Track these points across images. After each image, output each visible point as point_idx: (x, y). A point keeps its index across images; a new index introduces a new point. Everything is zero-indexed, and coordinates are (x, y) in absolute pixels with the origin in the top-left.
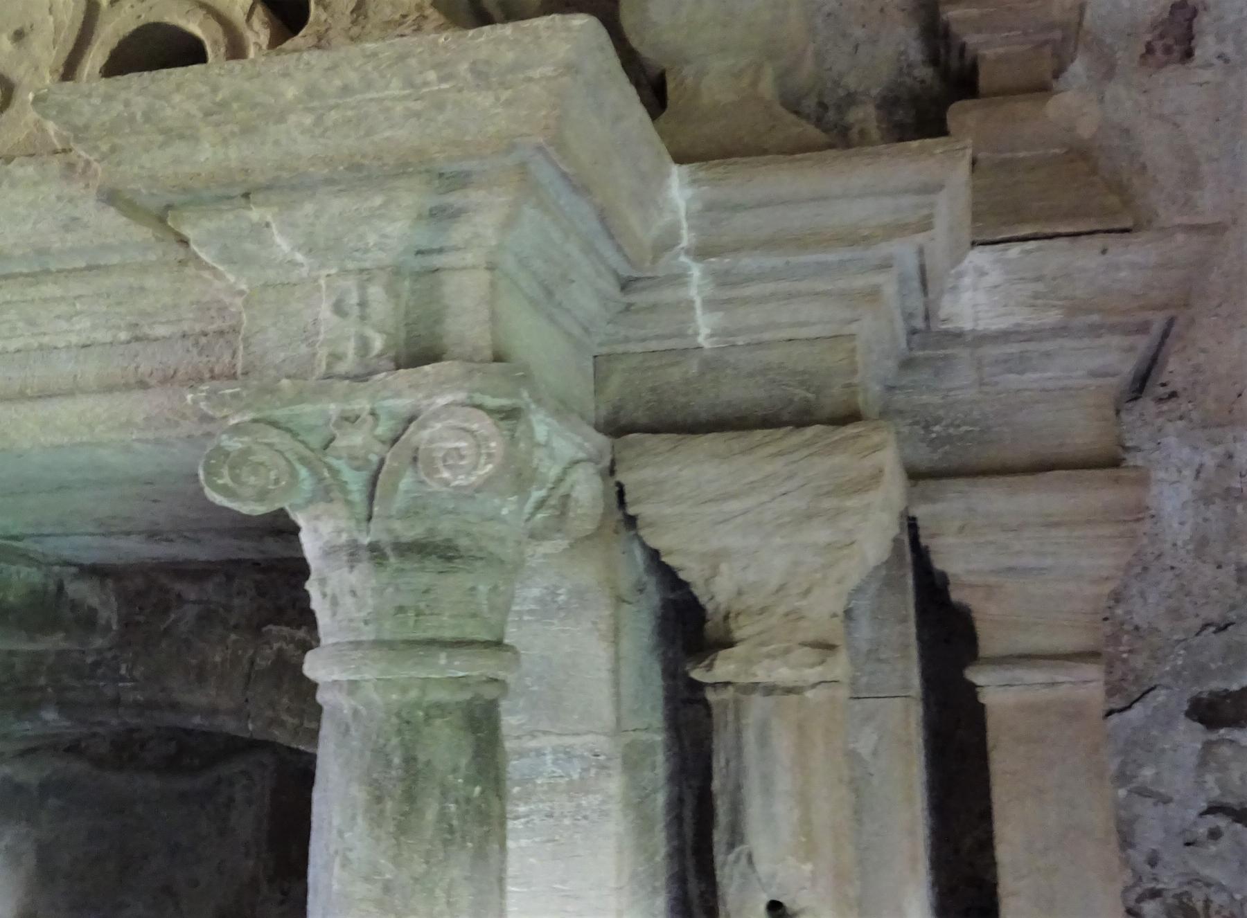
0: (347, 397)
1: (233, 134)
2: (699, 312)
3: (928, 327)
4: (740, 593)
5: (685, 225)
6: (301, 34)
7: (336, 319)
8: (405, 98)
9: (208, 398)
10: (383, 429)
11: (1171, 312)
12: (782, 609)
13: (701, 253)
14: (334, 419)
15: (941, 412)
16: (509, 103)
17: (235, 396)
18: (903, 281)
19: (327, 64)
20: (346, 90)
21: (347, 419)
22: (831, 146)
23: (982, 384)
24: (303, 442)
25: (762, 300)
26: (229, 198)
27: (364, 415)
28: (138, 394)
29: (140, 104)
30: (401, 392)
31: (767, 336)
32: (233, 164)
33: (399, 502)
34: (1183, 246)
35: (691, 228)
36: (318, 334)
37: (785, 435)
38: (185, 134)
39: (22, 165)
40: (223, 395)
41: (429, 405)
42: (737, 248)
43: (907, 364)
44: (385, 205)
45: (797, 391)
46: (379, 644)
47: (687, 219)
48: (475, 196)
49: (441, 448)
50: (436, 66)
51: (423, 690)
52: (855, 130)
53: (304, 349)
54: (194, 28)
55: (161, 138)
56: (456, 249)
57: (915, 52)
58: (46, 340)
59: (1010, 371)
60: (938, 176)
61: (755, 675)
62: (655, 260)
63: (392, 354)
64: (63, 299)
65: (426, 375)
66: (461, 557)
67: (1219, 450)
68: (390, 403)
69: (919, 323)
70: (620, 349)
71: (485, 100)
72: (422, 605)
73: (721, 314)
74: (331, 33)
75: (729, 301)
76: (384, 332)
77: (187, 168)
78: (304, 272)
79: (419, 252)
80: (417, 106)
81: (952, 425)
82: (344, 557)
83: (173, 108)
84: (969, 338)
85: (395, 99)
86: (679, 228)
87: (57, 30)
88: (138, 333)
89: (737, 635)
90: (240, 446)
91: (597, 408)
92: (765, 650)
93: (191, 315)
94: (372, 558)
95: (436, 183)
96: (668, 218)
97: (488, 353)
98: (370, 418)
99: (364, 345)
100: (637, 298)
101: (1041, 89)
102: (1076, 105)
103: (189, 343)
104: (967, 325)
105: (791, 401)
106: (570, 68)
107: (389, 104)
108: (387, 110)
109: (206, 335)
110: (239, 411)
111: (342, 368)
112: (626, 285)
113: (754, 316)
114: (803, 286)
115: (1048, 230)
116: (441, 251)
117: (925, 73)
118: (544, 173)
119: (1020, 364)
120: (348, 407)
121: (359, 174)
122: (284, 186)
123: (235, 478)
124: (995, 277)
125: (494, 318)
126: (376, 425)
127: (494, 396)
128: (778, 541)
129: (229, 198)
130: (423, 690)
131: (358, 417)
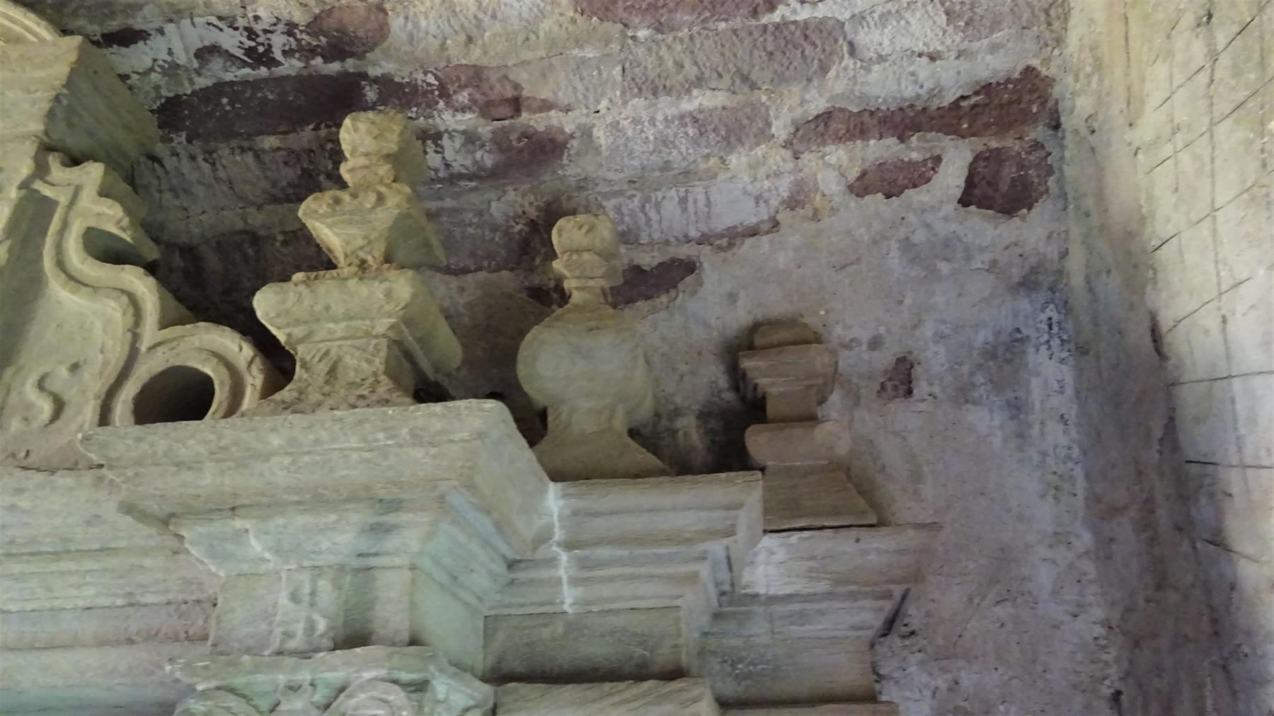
0: (294, 670)
1: (230, 468)
2: (565, 587)
3: (733, 591)
5: (557, 525)
6: (287, 388)
7: (291, 605)
8: (360, 449)
9: (181, 669)
10: (318, 697)
11: (906, 586)
13: (569, 545)
14: (282, 686)
15: (744, 654)
16: (434, 457)
17: (206, 667)
18: (715, 564)
19: (305, 424)
20: (317, 442)
21: (291, 688)
22: (662, 473)
23: (773, 632)
24: (254, 706)
25: (612, 579)
26: (220, 510)
27: (306, 685)
28: (124, 649)
29: (162, 445)
30: (336, 668)
31: (614, 606)
34: (912, 538)
35: (562, 527)
36: (275, 615)
38: (193, 465)
39: (63, 477)
41: (357, 678)
42: (597, 542)
43: (717, 616)
44: (337, 521)
48: (404, 517)
50: (384, 430)
52: (681, 433)
53: (263, 626)
54: (208, 371)
55: (175, 469)
56: (387, 553)
57: (723, 382)
58: (57, 603)
59: (792, 623)
60: (741, 495)
62: (535, 549)
63: (332, 634)
64: (77, 572)
67: (949, 676)
68: (327, 675)
69: (727, 588)
70: (505, 612)
71: (418, 453)
73: (581, 589)
74: (310, 389)
77: (191, 491)
78: (271, 566)
79: (360, 555)
80: (367, 455)
81: (751, 663)
84: (763, 599)
85: (352, 449)
86: (553, 525)
87: (105, 364)
88: (132, 601)
90: (203, 709)
91: (485, 658)
95: (377, 506)
96: (545, 520)
97: (405, 636)
98: (310, 688)
99: (311, 627)
100: (521, 575)
101: (810, 419)
102: (837, 430)
104: (762, 590)
105: (631, 658)
106: (480, 435)
107: (347, 453)
108: (346, 456)
110: (207, 679)
111: (292, 644)
112: (512, 565)
113: (607, 591)
114: (642, 570)
115: (818, 523)
116: (376, 554)
117: (729, 396)
118: (457, 499)
119: (802, 617)
122: (266, 505)
124: (781, 555)
125: (413, 605)
126: (312, 696)
129: (220, 510)
131: (300, 687)
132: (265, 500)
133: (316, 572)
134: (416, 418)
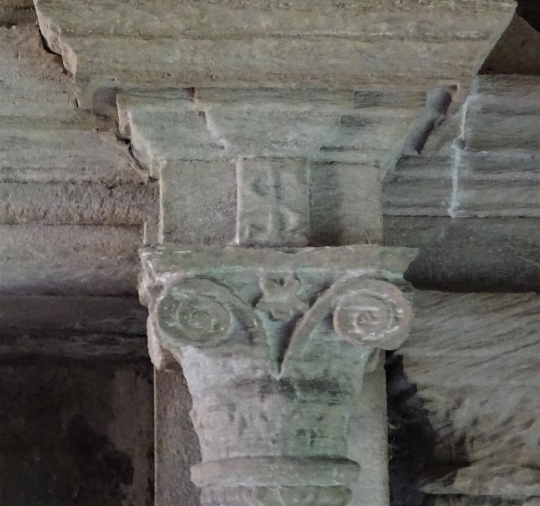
2: (455, 189)
4: (475, 422)
8: (357, 38)
12: (508, 437)
16: (436, 53)
20: (312, 27)
25: (509, 184)
27: (287, 279)
30: (320, 262)
31: (504, 213)
32: (199, 69)
33: (306, 348)
37: (530, 300)
38: (163, 38)
40: (177, 255)
41: (342, 275)
45: (527, 260)
46: (286, 458)
47: (467, 117)
48: (381, 112)
49: (357, 311)
50: (389, 21)
51: (316, 496)
61: (486, 489)
65: (350, 252)
66: (340, 392)
68: (308, 270)
71: (420, 48)
72: (316, 430)
73: (473, 192)
75: (480, 182)
76: (298, 211)
82: (257, 389)
83: (162, 21)
85: (346, 37)
89: (473, 456)
92: (494, 469)
93: (64, 165)
94: (282, 392)
99: (281, 223)
103: (59, 188)
109: (74, 183)
113: (499, 196)
116: (341, 149)
120: (273, 271)
121: (306, 88)
123: (184, 322)
127: (393, 272)
128: (513, 382)
130: (316, 496)
132: (245, 85)
133: (278, 164)
134: (428, 11)
